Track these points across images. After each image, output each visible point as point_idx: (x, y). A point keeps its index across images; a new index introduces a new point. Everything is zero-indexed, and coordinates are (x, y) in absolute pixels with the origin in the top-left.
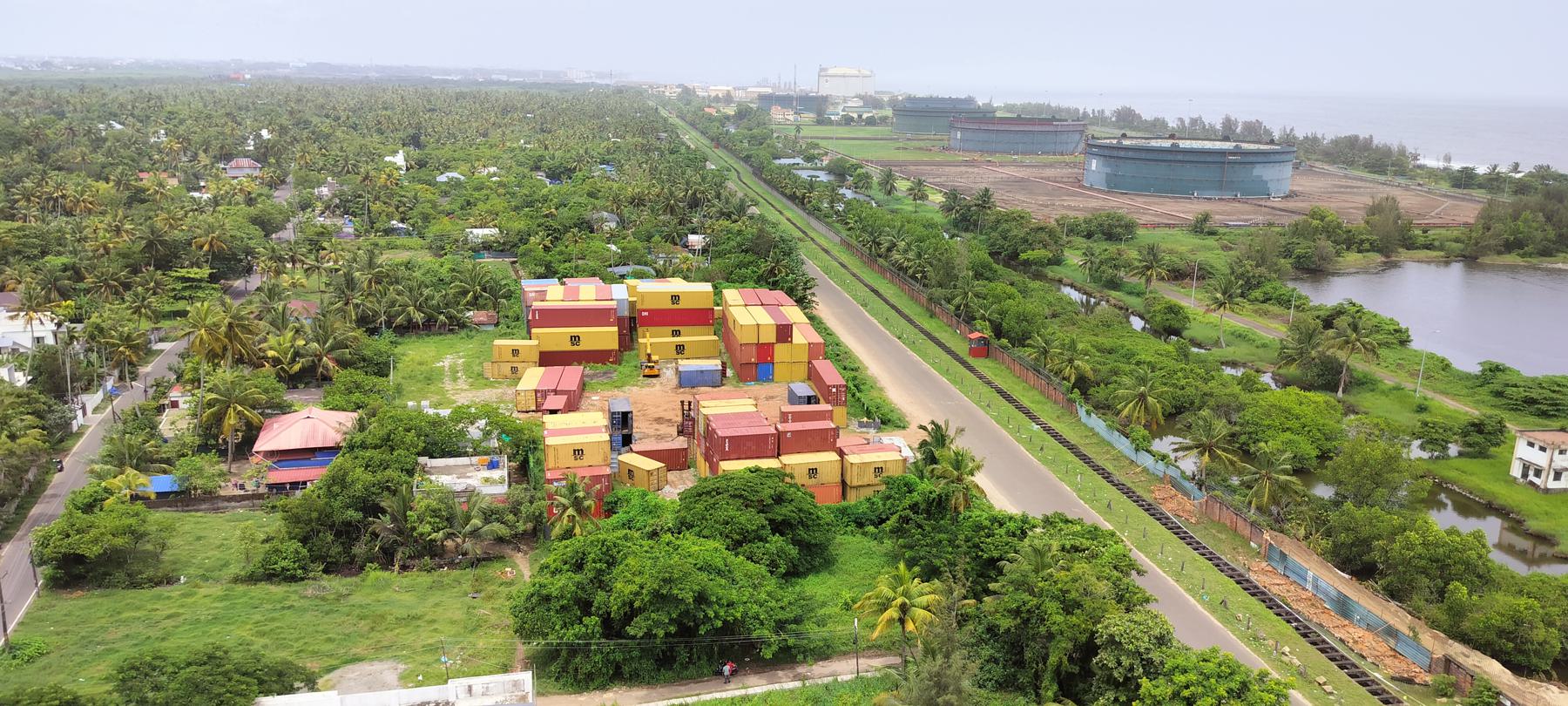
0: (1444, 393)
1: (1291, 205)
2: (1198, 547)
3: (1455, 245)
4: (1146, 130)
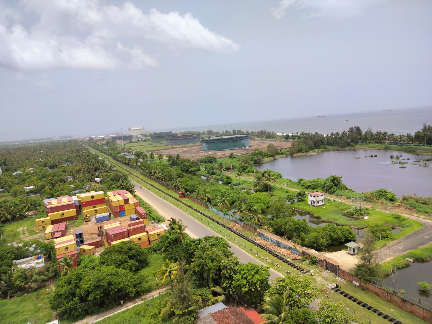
0: (291, 187)
1: (251, 148)
2: (243, 237)
4: (215, 135)
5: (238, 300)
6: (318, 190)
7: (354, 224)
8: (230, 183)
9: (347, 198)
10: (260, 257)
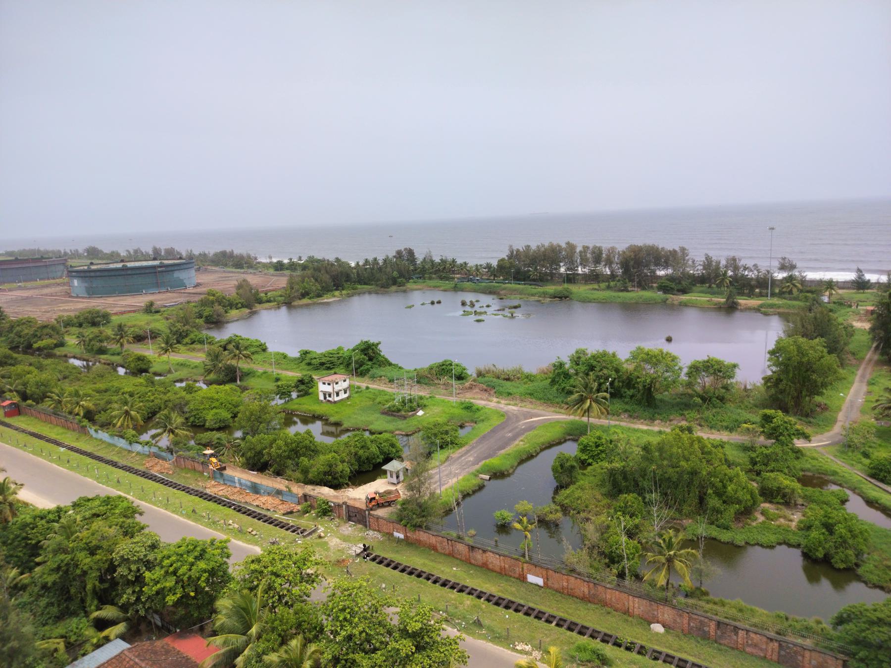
0: (286, 369)
1: (198, 290)
2: (175, 486)
3: (280, 298)
4: (107, 259)
5: (159, 624)
6: (337, 370)
7: (400, 427)
8: (146, 371)
9: (390, 381)
10: (214, 523)
